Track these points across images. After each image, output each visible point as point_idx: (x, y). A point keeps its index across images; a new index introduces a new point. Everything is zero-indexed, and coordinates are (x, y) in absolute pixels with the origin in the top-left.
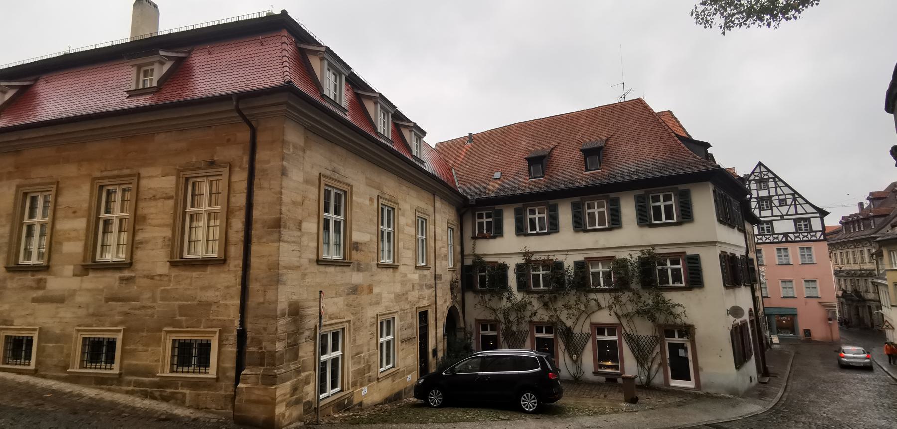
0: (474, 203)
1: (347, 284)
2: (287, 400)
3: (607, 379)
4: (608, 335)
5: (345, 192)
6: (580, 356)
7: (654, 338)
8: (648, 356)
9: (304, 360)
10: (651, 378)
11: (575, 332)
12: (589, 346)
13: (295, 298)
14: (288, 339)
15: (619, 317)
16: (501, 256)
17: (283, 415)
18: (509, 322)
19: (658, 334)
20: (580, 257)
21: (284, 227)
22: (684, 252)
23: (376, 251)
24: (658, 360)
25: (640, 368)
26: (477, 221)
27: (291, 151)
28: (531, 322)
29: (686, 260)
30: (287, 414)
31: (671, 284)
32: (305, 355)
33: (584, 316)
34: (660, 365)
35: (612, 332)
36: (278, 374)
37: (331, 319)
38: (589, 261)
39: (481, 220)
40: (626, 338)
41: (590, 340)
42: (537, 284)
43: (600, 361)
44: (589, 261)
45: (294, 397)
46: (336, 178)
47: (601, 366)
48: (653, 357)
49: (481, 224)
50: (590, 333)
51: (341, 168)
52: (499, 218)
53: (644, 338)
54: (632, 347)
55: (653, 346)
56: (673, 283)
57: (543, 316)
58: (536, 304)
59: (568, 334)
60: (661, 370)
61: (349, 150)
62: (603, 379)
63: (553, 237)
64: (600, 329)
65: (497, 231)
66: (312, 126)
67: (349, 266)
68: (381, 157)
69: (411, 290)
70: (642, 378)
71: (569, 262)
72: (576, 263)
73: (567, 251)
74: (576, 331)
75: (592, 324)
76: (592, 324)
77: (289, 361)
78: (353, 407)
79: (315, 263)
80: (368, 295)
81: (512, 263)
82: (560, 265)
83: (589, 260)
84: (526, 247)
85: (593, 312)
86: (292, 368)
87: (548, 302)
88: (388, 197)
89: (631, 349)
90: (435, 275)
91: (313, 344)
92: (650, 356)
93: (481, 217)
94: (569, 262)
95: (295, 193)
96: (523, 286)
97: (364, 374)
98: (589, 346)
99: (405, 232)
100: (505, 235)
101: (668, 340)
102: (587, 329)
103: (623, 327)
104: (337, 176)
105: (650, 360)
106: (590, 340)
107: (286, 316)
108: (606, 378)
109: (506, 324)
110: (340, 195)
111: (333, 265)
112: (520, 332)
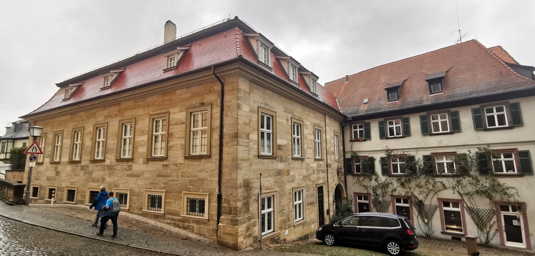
1: (275, 169)
3: (453, 238)
5: (300, 125)
6: (431, 220)
10: (490, 238)
12: (437, 213)
15: (461, 195)
19: (494, 209)
23: (291, 150)
24: (495, 227)
26: (353, 130)
27: (242, 94)
34: (497, 230)
41: (438, 210)
43: (446, 224)
45: (248, 233)
46: (267, 108)
47: (447, 229)
50: (438, 205)
54: (473, 217)
55: (491, 217)
56: (507, 171)
57: (401, 191)
58: (395, 184)
59: (420, 205)
60: (498, 234)
61: (274, 91)
62: (450, 237)
63: (406, 139)
70: (482, 239)
73: (418, 148)
74: (427, 203)
82: (412, 158)
84: (387, 146)
87: (404, 183)
92: (488, 224)
94: (419, 156)
96: (385, 172)
98: (437, 213)
99: (308, 138)
100: (372, 139)
102: (435, 202)
104: (267, 107)
105: (488, 226)
106: (438, 210)
107: (242, 187)
108: (452, 237)
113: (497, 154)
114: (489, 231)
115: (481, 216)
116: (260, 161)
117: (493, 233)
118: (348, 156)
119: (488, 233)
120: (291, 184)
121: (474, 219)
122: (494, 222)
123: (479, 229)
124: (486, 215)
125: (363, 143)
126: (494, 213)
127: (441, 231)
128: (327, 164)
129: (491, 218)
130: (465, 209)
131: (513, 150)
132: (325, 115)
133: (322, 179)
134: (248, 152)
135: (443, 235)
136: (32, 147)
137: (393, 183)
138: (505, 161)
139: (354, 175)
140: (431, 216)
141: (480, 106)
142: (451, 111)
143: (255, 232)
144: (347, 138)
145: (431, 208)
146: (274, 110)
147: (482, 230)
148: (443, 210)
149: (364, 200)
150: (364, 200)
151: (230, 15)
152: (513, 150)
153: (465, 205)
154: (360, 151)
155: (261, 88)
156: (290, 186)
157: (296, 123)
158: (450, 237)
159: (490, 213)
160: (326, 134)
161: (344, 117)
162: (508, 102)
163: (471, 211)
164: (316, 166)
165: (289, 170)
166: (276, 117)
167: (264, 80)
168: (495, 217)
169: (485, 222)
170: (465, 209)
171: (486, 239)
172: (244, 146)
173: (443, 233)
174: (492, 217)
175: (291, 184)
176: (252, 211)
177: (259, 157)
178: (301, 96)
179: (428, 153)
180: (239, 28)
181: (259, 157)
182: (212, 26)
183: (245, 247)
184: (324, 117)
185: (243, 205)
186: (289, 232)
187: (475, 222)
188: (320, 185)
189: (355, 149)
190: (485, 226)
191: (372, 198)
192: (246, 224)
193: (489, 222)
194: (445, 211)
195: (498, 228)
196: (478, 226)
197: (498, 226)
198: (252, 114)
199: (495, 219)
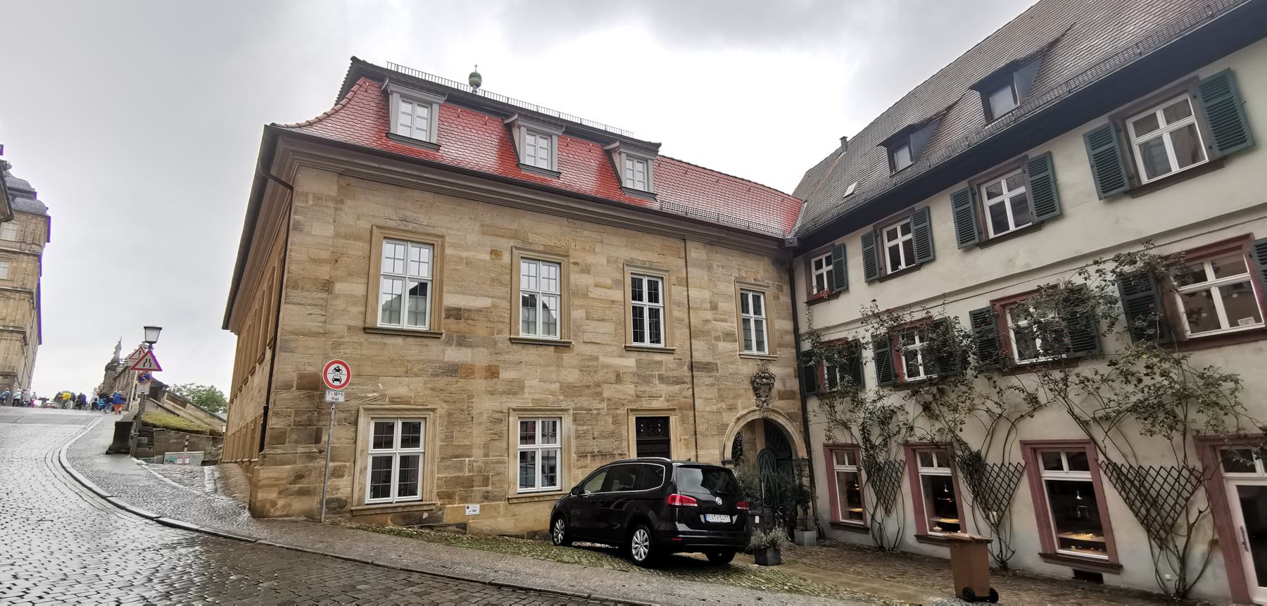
0: (796, 244)
1: (433, 362)
2: (282, 488)
3: (1079, 575)
4: (1070, 469)
5: (764, 293)
6: (1007, 513)
7: (1185, 473)
8: (1175, 521)
9: (334, 447)
10: (1190, 578)
11: (990, 460)
12: (1024, 492)
13: (310, 369)
14: (295, 416)
15: (1084, 424)
16: (850, 327)
17: (274, 504)
18: (873, 447)
19: (1195, 462)
20: (981, 302)
21: (294, 288)
22: (1247, 237)
23: (508, 322)
24: (1206, 532)
25: (1157, 550)
26: (815, 273)
27: (311, 202)
28: (906, 444)
29: (1255, 255)
30: (281, 503)
31: (1226, 327)
32: (335, 441)
33: (1004, 427)
34: (1213, 543)
35: (1079, 462)
36: (269, 454)
37: (393, 402)
38: (1004, 306)
39: (819, 272)
40: (1109, 474)
41: (1025, 481)
42: (913, 372)
43: (1061, 527)
44: (1004, 306)
45: (298, 486)
46: (410, 228)
47: (1066, 544)
48: (1192, 521)
49: (820, 277)
50: (1023, 463)
51: (421, 216)
52: (1130, 297)
53: (1163, 473)
54: (1128, 497)
55: (1185, 494)
56: (1233, 323)
57: (925, 430)
58: (913, 410)
59: (975, 465)
60: (1219, 558)
61: (437, 191)
62: (1067, 572)
63: (926, 271)
64: (1047, 453)
65: (839, 285)
66: (347, 170)
67: (439, 338)
68: (440, 181)
69: (613, 381)
70: (1168, 576)
71: (961, 315)
72: (977, 317)
73: (944, 296)
74: (993, 459)
75: (1024, 444)
76: (1024, 444)
77: (296, 442)
78: (440, 526)
79: (362, 332)
80: (486, 379)
81: (864, 334)
82: (942, 327)
83: (1003, 303)
84: (874, 301)
85: (1022, 416)
86: (299, 451)
87: (931, 403)
88: (541, 248)
89: (1125, 501)
90: (692, 362)
91: (353, 429)
92: (1181, 520)
93: (819, 266)
94: (961, 315)
95: (316, 248)
96: (888, 377)
97: (473, 487)
98: (1024, 492)
99: (591, 295)
100: (851, 287)
101: (1234, 482)
102: (1016, 456)
103: (1099, 447)
104: (410, 226)
105: (1184, 531)
106: (1025, 481)
107: (294, 389)
108: (1076, 572)
109: (866, 450)
110: (759, 297)
111: (401, 335)
112: (888, 462)
113: (1188, 265)
114: (1186, 547)
115: (1154, 494)
116: (372, 340)
117: (1203, 554)
118: (807, 346)
119: (1183, 560)
120: (505, 400)
121: (1131, 506)
122: (1200, 512)
123: (1153, 542)
124: (1167, 487)
125: (834, 303)
126: (1199, 481)
127: (1041, 552)
128: (692, 362)
129: (1187, 499)
130: (1102, 473)
131: (1238, 244)
132: (684, 240)
133: (663, 398)
134: (323, 319)
135: (1048, 564)
136: (144, 360)
137: (907, 408)
138: (1222, 289)
139: (821, 396)
140: (1005, 502)
141: (1109, 117)
142: (1030, 157)
143: (338, 489)
144: (802, 297)
145: (1002, 475)
146: (437, 231)
147: (1163, 544)
148: (1043, 479)
149: (849, 464)
150: (849, 464)
151: (476, 66)
152: (1238, 244)
153: (1101, 458)
154: (828, 328)
155: (388, 187)
156: (499, 404)
157: (644, 275)
158: (1067, 572)
159: (1183, 481)
160: (688, 287)
161: (778, 243)
162: (1197, 77)
163: (1116, 472)
164: (635, 365)
165: (498, 366)
166: (443, 246)
167: (403, 173)
168: (1201, 494)
169: (1169, 515)
170: (1102, 473)
171: (1180, 576)
172: (309, 305)
173: (1048, 556)
174: (1192, 494)
175: (505, 400)
176: (333, 443)
177: (367, 331)
178: (537, 194)
179: (982, 303)
180: (364, 76)
181: (367, 331)
182: (504, 101)
183: (285, 513)
184: (683, 245)
185: (294, 425)
186: (480, 510)
187: (1137, 515)
188: (648, 413)
189: (817, 325)
190: (1171, 529)
191: (862, 455)
192: (292, 466)
193: (1184, 513)
194: (1051, 484)
195: (1217, 537)
196: (1148, 531)
197: (1216, 527)
198: (349, 241)
199: (1200, 501)
